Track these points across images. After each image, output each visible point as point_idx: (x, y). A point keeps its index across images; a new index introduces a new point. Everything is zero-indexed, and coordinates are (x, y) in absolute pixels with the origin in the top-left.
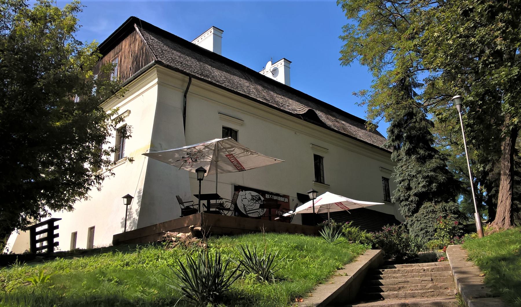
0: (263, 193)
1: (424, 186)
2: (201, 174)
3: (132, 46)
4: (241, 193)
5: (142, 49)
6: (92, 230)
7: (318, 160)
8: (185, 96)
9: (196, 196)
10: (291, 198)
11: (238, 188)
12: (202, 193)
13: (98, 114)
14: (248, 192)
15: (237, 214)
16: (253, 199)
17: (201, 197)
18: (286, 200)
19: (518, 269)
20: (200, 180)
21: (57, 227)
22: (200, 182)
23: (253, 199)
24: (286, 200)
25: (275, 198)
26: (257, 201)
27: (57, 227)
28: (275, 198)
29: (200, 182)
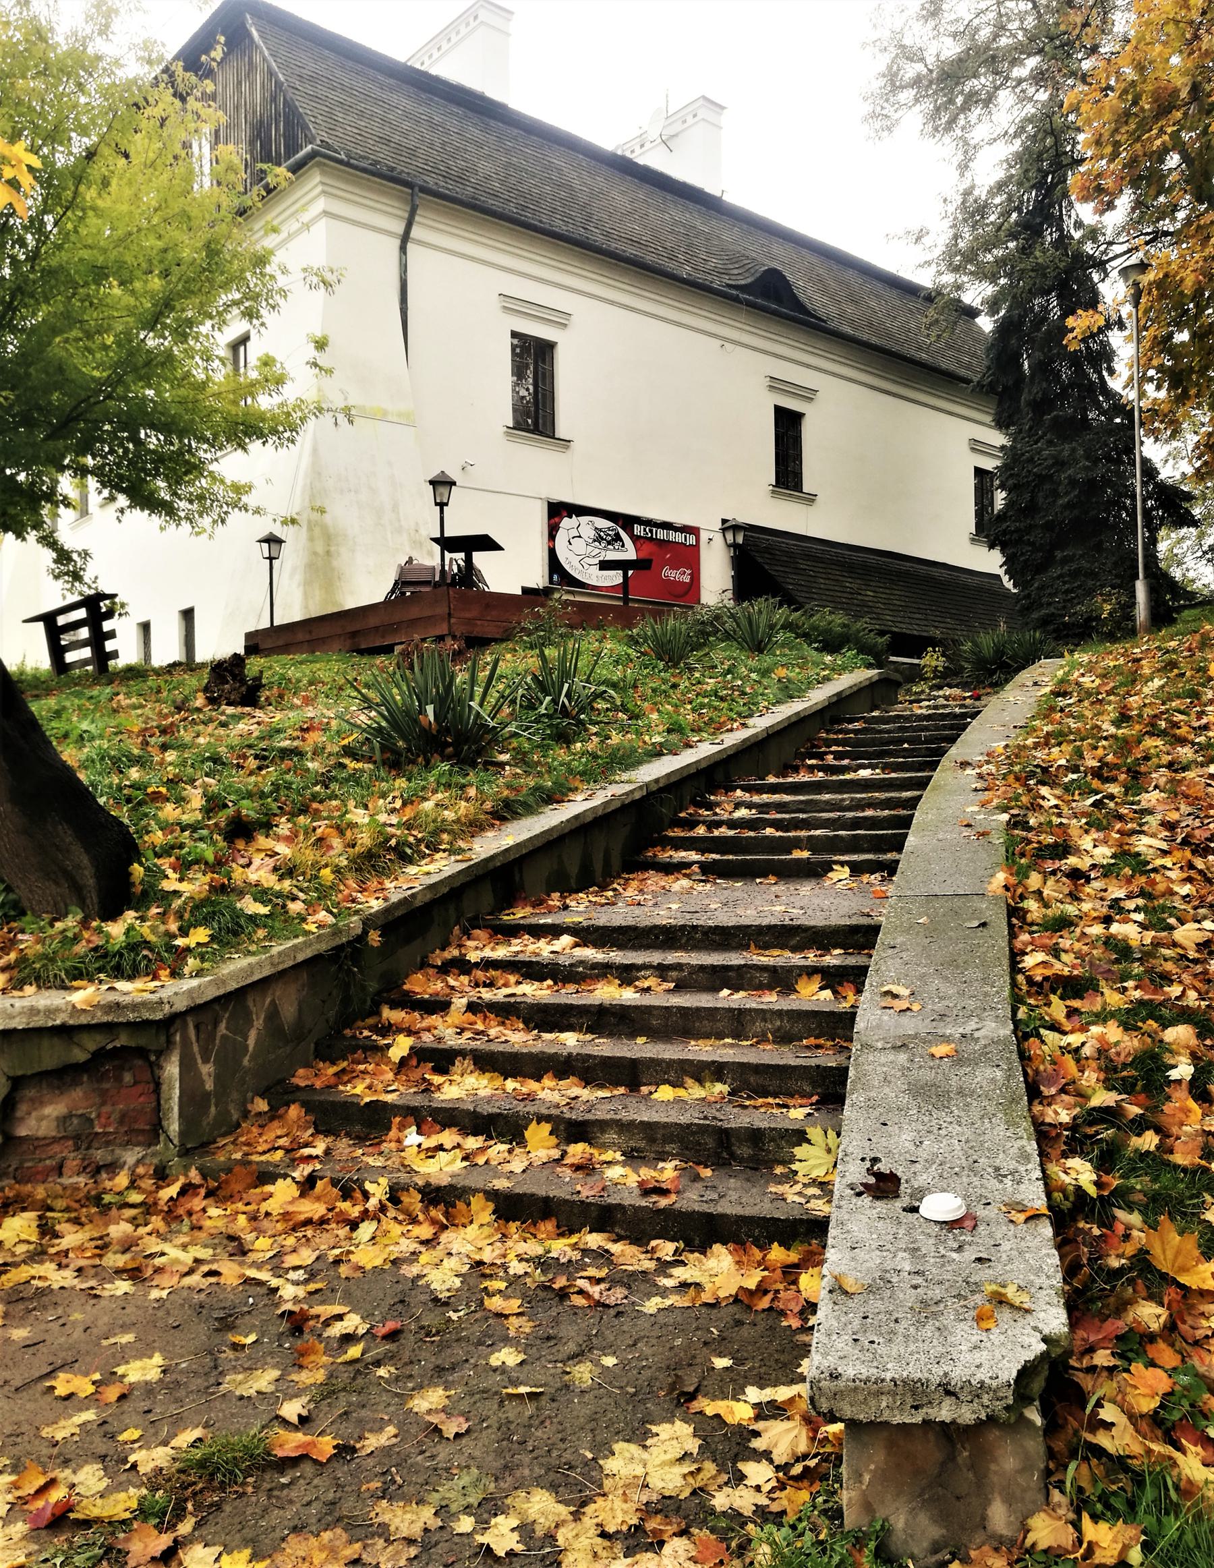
0: (626, 521)
1: (1069, 506)
2: (443, 490)
3: (245, 87)
4: (566, 523)
5: (274, 99)
6: (188, 615)
7: (788, 426)
8: (403, 249)
9: (434, 540)
10: (704, 536)
11: (558, 511)
12: (448, 533)
13: (165, 495)
14: (584, 520)
15: (555, 577)
16: (599, 539)
17: (447, 544)
18: (691, 540)
19: (1206, 727)
20: (442, 505)
21: (112, 635)
22: (442, 512)
23: (599, 539)
24: (691, 540)
25: (661, 534)
26: (609, 543)
27: (112, 635)
28: (661, 534)
29: (442, 512)
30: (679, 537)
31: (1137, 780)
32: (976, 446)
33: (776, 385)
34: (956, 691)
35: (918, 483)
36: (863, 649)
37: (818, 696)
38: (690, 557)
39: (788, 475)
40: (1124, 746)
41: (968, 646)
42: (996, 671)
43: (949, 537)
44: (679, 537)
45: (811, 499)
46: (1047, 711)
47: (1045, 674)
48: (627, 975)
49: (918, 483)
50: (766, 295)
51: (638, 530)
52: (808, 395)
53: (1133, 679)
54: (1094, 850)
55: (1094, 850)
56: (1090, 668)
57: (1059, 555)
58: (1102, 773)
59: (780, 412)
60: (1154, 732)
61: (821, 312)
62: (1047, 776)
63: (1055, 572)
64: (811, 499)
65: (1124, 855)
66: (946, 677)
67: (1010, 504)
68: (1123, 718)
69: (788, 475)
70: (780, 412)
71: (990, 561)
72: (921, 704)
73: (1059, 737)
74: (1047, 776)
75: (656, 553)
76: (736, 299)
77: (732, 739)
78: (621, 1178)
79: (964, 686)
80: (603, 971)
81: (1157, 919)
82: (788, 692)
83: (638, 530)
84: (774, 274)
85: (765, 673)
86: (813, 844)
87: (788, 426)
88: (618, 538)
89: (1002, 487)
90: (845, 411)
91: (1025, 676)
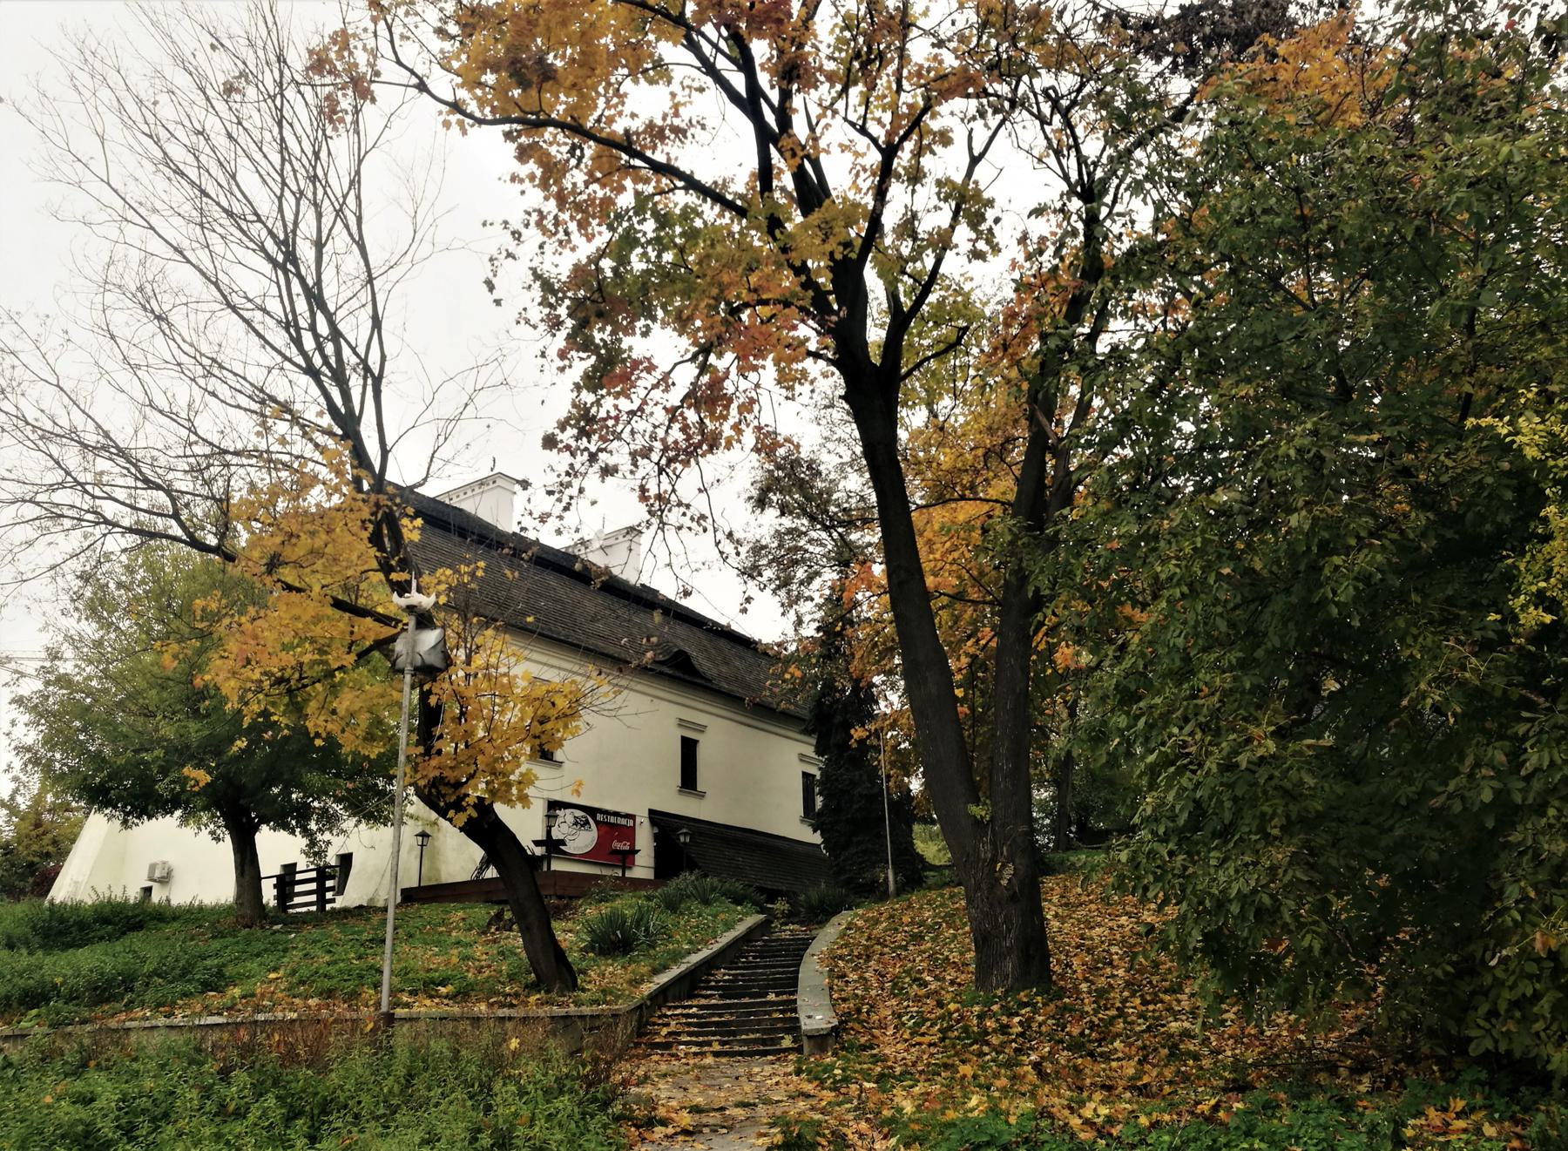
7: (689, 749)
10: (638, 820)
16: (576, 824)
18: (631, 823)
23: (576, 824)
25: (612, 820)
30: (623, 821)
31: (869, 958)
32: (803, 758)
33: (682, 723)
34: (796, 927)
35: (767, 784)
36: (755, 903)
37: (740, 929)
38: (629, 834)
39: (689, 780)
40: (867, 948)
41: (802, 898)
42: (820, 914)
43: (787, 819)
44: (623, 821)
45: (702, 795)
46: (843, 935)
47: (844, 918)
48: (720, 1015)
49: (767, 784)
50: (676, 667)
51: (599, 817)
52: (701, 729)
53: (877, 922)
54: (853, 976)
55: (853, 976)
56: (861, 917)
57: (855, 839)
58: (859, 957)
59: (684, 739)
60: (879, 943)
61: (708, 674)
62: (841, 958)
63: (853, 850)
64: (702, 795)
65: (861, 977)
66: (790, 917)
67: (825, 806)
68: (869, 938)
69: (689, 780)
70: (684, 739)
71: (817, 838)
72: (788, 931)
73: (846, 945)
74: (841, 958)
75: (613, 830)
76: (661, 673)
77: (716, 947)
78: (737, 1048)
79: (801, 923)
80: (713, 1015)
81: (866, 989)
82: (729, 926)
83: (599, 817)
84: (681, 653)
85: (715, 916)
86: (759, 987)
87: (689, 749)
88: (587, 822)
89: (820, 793)
90: (722, 736)
91: (835, 920)
